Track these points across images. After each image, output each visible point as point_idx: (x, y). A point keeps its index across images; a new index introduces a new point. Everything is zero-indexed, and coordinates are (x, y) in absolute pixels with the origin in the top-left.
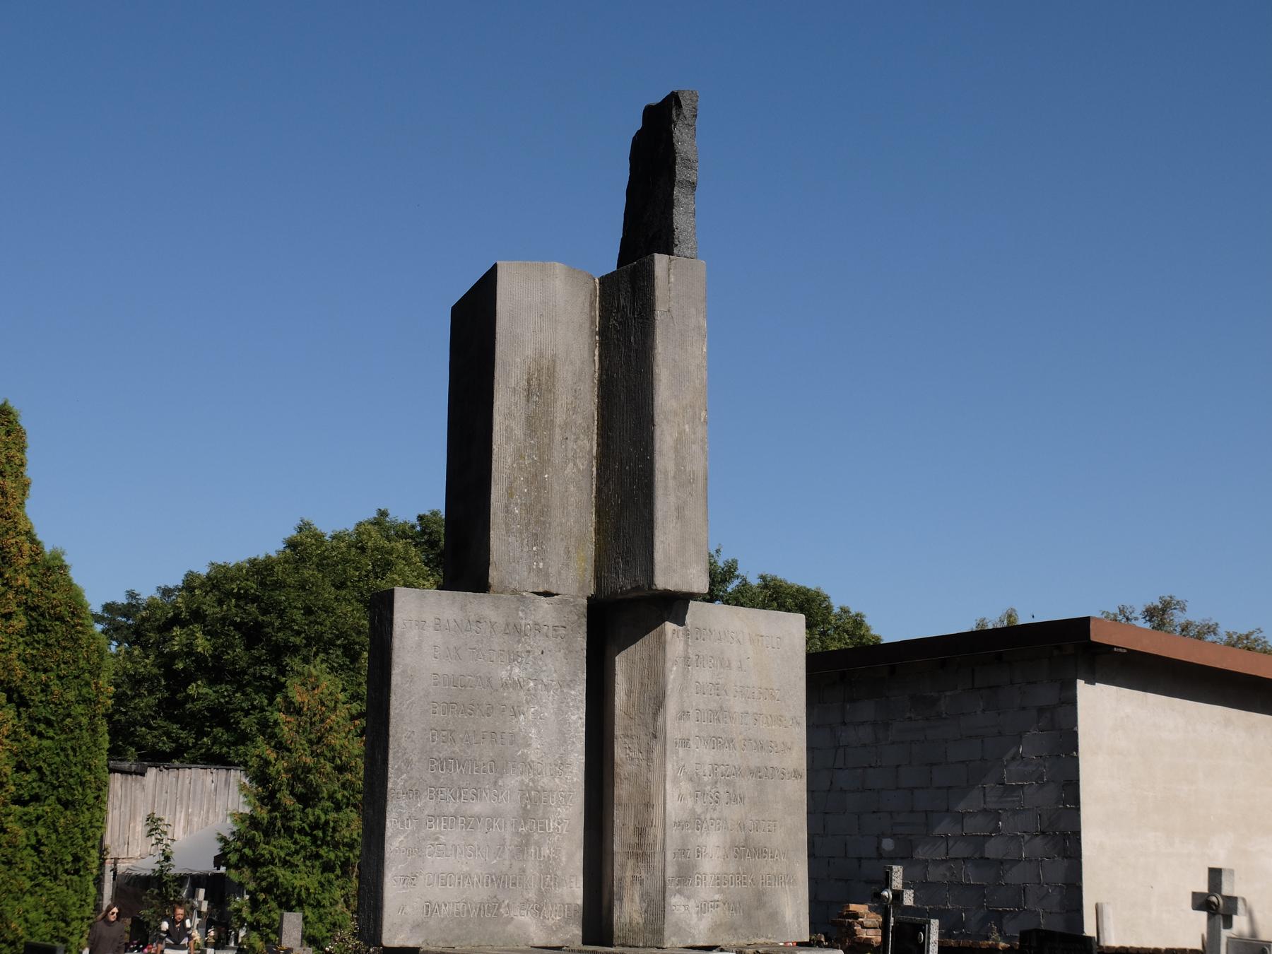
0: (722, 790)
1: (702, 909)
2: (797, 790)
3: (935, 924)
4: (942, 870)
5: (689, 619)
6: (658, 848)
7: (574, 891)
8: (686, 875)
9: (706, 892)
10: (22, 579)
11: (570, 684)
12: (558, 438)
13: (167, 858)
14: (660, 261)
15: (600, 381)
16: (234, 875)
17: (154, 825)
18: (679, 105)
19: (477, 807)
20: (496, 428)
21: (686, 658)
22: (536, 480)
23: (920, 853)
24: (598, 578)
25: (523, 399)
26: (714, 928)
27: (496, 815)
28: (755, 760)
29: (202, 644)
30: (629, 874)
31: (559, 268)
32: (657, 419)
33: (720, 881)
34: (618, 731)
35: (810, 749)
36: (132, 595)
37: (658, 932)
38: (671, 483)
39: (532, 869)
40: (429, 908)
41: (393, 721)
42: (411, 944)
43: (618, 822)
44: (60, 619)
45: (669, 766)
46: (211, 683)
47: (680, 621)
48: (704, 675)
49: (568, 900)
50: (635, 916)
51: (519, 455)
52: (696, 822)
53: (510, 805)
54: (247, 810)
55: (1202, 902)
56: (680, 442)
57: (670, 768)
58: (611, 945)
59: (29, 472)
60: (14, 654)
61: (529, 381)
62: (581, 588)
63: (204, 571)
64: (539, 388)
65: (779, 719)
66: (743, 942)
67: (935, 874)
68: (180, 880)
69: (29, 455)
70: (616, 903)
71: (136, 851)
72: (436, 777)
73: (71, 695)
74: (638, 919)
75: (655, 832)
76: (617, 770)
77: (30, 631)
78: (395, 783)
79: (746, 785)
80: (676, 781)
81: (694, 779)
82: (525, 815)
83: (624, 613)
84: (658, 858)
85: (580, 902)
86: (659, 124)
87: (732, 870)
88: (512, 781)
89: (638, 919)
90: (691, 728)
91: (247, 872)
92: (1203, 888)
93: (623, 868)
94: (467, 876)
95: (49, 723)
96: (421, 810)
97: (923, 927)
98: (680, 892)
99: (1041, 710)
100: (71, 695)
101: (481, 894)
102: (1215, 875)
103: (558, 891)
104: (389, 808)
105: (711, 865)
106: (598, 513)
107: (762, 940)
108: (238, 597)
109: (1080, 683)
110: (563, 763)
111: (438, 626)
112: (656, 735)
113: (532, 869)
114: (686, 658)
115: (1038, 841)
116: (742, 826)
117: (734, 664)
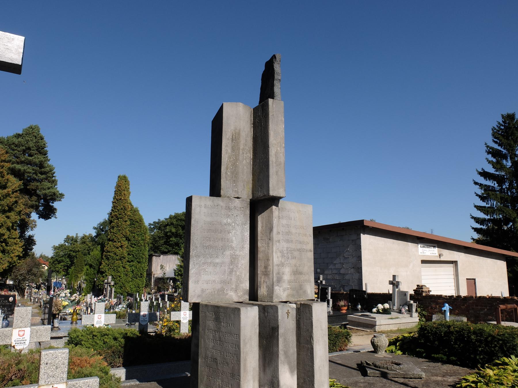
0: (290, 255)
1: (284, 290)
2: (311, 255)
3: (330, 288)
4: (331, 276)
5: (279, 205)
6: (271, 272)
7: (246, 285)
8: (279, 280)
9: (285, 285)
10: (129, 213)
11: (245, 224)
12: (241, 153)
13: (164, 274)
14: (270, 101)
15: (253, 137)
16: (176, 277)
17: (162, 267)
18: (275, 58)
19: (217, 261)
20: (223, 150)
21: (279, 217)
22: (235, 165)
23: (326, 272)
24: (253, 194)
25: (231, 142)
26: (288, 296)
27: (223, 263)
28: (299, 246)
29: (174, 230)
30: (262, 280)
31: (241, 104)
32: (270, 146)
33: (289, 282)
34: (259, 238)
35: (314, 244)
36: (159, 220)
37: (272, 297)
38: (274, 164)
39: (234, 279)
40: (203, 291)
41: (192, 235)
42: (197, 302)
43: (259, 264)
44: (137, 222)
45: (274, 248)
46: (175, 238)
47: (277, 205)
48: (284, 222)
49: (245, 288)
50: (265, 292)
51: (229, 158)
52: (282, 265)
53: (227, 260)
54: (179, 264)
55: (391, 283)
56: (277, 153)
57: (274, 249)
58: (257, 301)
59: (130, 190)
60: (127, 229)
61: (232, 136)
62: (248, 197)
63: (173, 215)
64: (235, 138)
65: (306, 235)
66: (296, 300)
67: (329, 277)
68: (168, 278)
69: (130, 186)
70: (259, 289)
71: (158, 272)
72: (205, 252)
73: (140, 239)
74: (265, 293)
75: (270, 267)
76: (259, 249)
77: (131, 224)
78: (192, 253)
79: (296, 254)
80: (276, 252)
81: (282, 252)
82: (232, 263)
83: (261, 203)
84: (271, 275)
85: (248, 288)
86: (269, 66)
87: (293, 278)
88: (228, 253)
89: (265, 293)
90: (280, 237)
91: (180, 277)
92: (392, 280)
93: (261, 278)
94: (214, 281)
95: (135, 245)
96: (200, 261)
97: (327, 289)
98: (278, 285)
99: (353, 240)
100: (140, 239)
101: (218, 286)
102: (394, 277)
103: (242, 285)
104: (190, 261)
105: (287, 277)
106: (253, 175)
107: (301, 299)
108: (180, 220)
109: (362, 234)
110: (243, 247)
111: (205, 207)
112: (270, 239)
113: (234, 279)
114: (279, 217)
115: (352, 270)
116: (295, 266)
117: (293, 219)
